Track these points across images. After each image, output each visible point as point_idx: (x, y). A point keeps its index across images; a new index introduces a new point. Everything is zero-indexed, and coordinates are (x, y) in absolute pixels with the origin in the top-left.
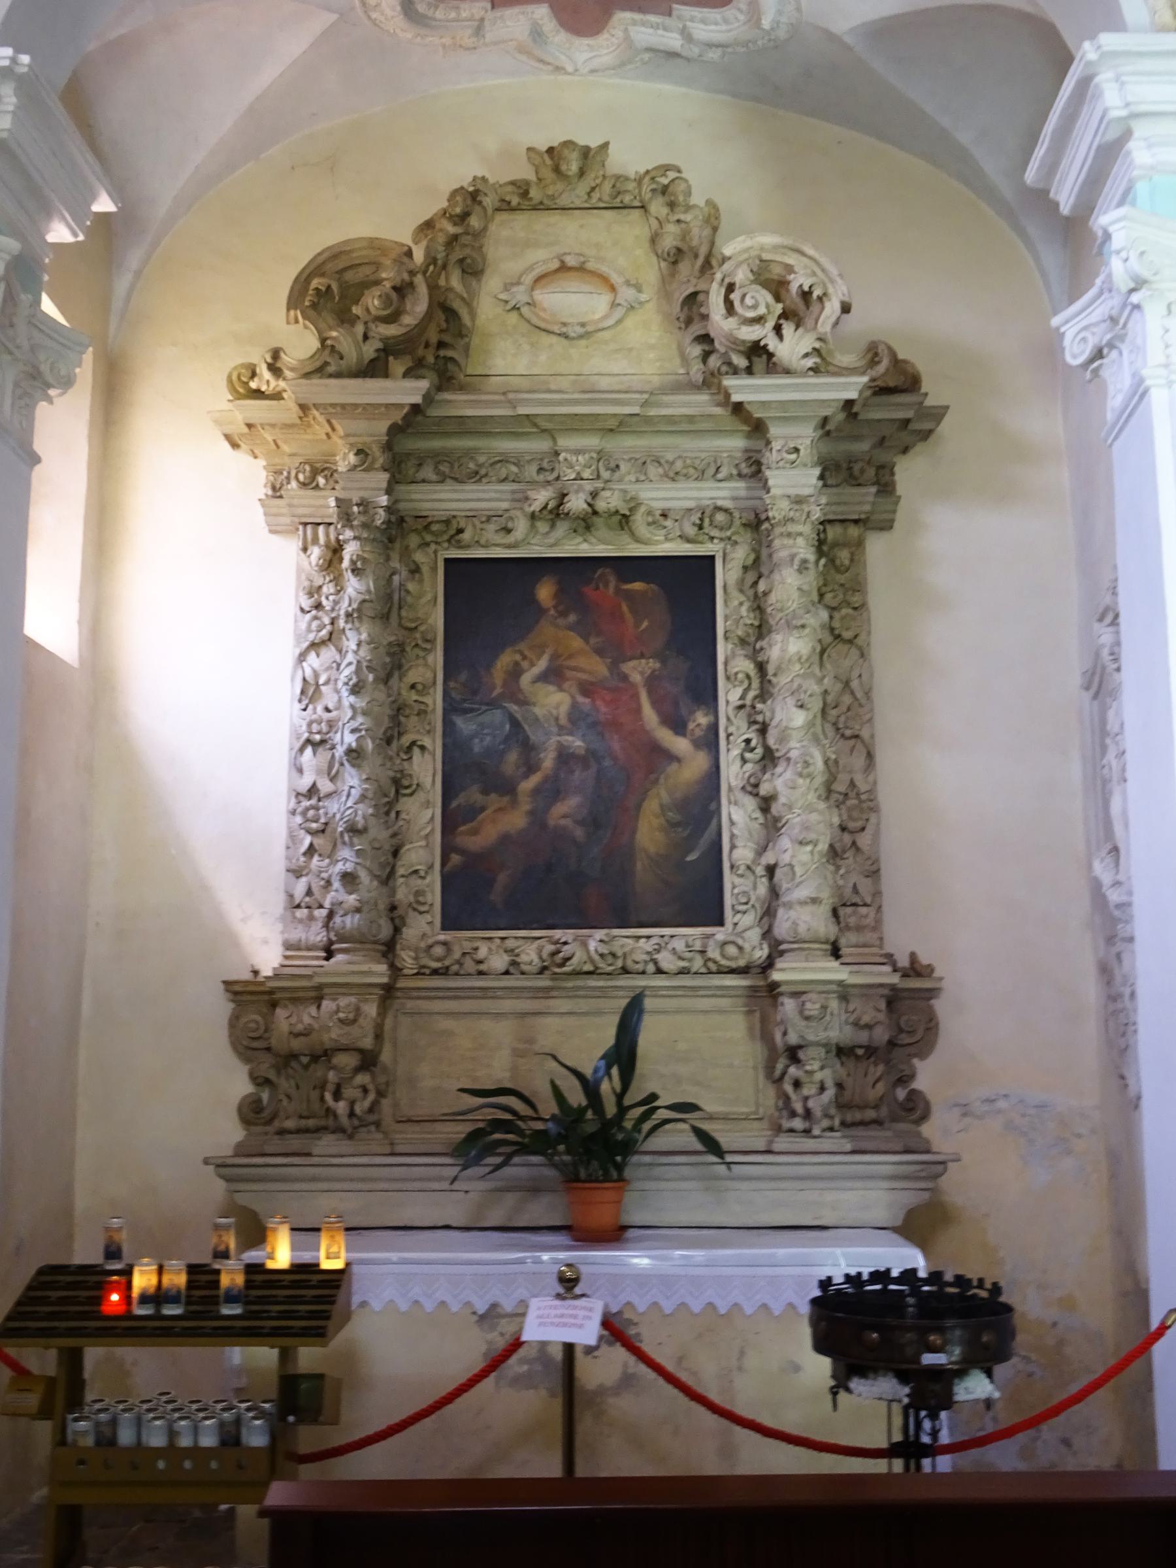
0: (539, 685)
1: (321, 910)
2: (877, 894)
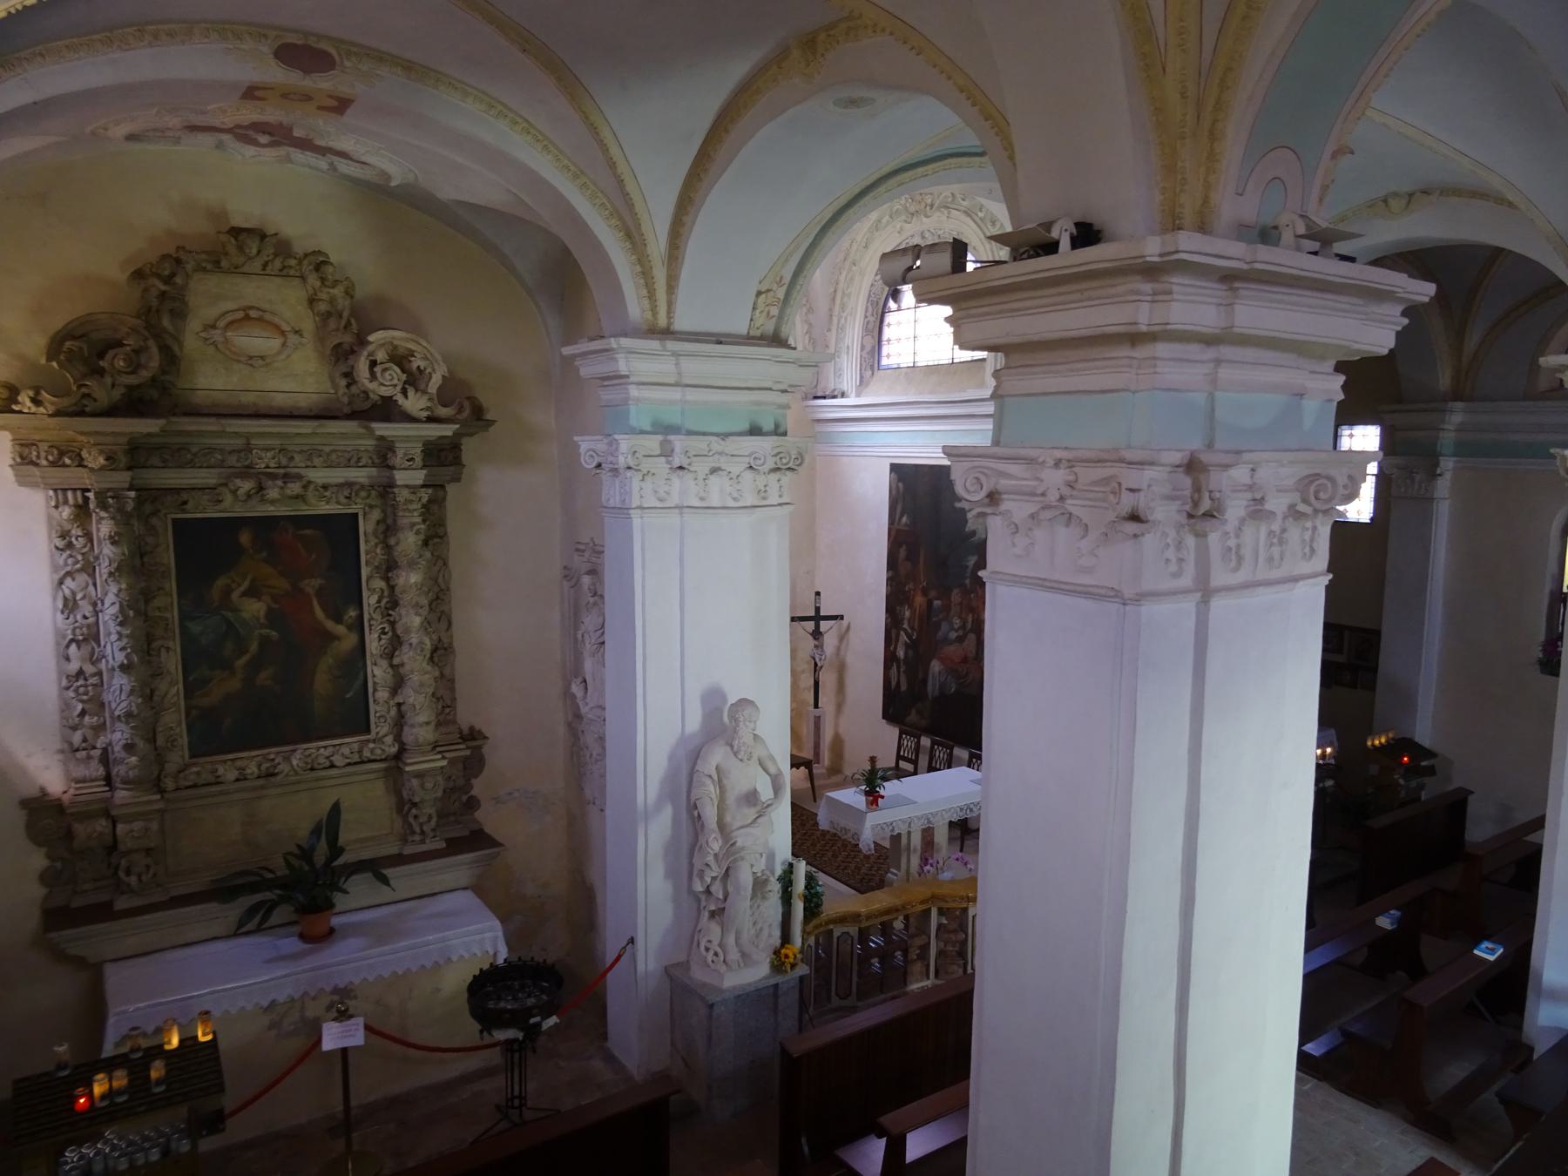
0: (244, 598)
1: (96, 751)
2: (454, 699)
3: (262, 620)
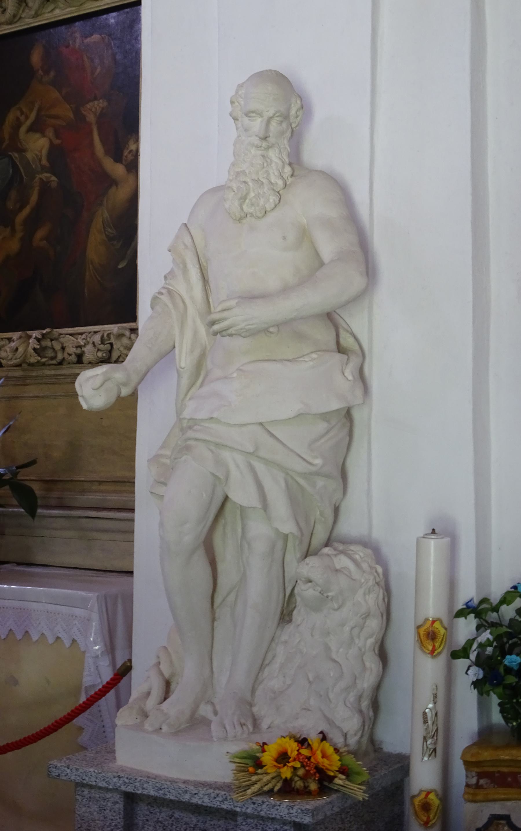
3: (44, 162)
